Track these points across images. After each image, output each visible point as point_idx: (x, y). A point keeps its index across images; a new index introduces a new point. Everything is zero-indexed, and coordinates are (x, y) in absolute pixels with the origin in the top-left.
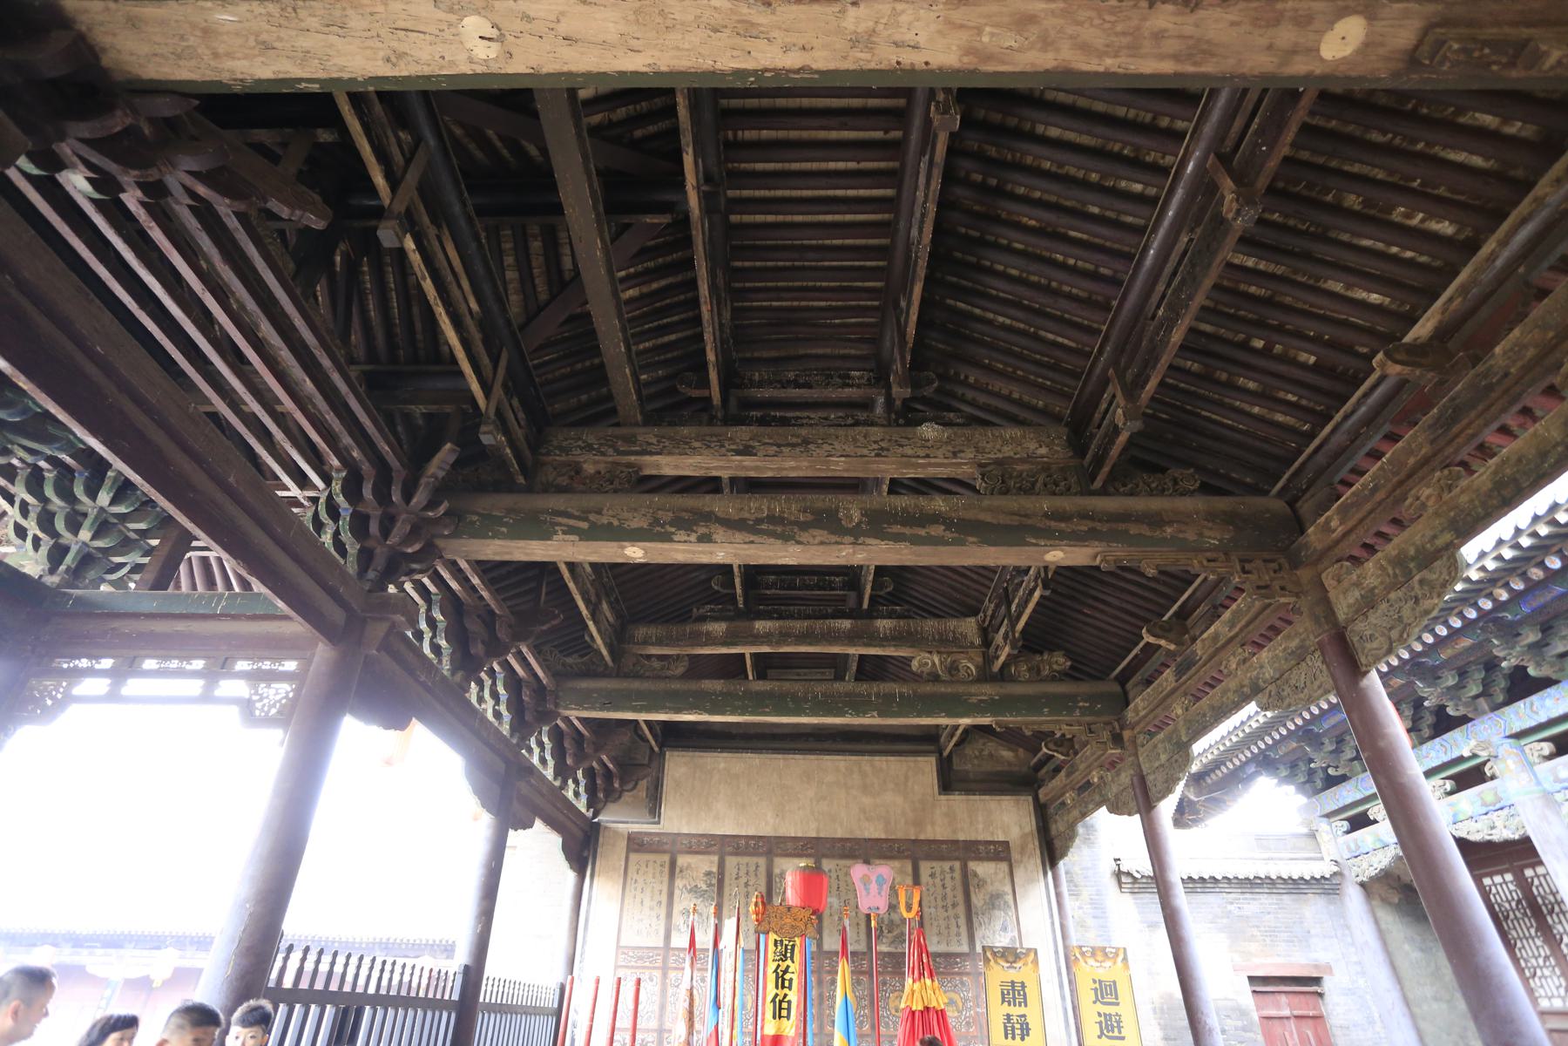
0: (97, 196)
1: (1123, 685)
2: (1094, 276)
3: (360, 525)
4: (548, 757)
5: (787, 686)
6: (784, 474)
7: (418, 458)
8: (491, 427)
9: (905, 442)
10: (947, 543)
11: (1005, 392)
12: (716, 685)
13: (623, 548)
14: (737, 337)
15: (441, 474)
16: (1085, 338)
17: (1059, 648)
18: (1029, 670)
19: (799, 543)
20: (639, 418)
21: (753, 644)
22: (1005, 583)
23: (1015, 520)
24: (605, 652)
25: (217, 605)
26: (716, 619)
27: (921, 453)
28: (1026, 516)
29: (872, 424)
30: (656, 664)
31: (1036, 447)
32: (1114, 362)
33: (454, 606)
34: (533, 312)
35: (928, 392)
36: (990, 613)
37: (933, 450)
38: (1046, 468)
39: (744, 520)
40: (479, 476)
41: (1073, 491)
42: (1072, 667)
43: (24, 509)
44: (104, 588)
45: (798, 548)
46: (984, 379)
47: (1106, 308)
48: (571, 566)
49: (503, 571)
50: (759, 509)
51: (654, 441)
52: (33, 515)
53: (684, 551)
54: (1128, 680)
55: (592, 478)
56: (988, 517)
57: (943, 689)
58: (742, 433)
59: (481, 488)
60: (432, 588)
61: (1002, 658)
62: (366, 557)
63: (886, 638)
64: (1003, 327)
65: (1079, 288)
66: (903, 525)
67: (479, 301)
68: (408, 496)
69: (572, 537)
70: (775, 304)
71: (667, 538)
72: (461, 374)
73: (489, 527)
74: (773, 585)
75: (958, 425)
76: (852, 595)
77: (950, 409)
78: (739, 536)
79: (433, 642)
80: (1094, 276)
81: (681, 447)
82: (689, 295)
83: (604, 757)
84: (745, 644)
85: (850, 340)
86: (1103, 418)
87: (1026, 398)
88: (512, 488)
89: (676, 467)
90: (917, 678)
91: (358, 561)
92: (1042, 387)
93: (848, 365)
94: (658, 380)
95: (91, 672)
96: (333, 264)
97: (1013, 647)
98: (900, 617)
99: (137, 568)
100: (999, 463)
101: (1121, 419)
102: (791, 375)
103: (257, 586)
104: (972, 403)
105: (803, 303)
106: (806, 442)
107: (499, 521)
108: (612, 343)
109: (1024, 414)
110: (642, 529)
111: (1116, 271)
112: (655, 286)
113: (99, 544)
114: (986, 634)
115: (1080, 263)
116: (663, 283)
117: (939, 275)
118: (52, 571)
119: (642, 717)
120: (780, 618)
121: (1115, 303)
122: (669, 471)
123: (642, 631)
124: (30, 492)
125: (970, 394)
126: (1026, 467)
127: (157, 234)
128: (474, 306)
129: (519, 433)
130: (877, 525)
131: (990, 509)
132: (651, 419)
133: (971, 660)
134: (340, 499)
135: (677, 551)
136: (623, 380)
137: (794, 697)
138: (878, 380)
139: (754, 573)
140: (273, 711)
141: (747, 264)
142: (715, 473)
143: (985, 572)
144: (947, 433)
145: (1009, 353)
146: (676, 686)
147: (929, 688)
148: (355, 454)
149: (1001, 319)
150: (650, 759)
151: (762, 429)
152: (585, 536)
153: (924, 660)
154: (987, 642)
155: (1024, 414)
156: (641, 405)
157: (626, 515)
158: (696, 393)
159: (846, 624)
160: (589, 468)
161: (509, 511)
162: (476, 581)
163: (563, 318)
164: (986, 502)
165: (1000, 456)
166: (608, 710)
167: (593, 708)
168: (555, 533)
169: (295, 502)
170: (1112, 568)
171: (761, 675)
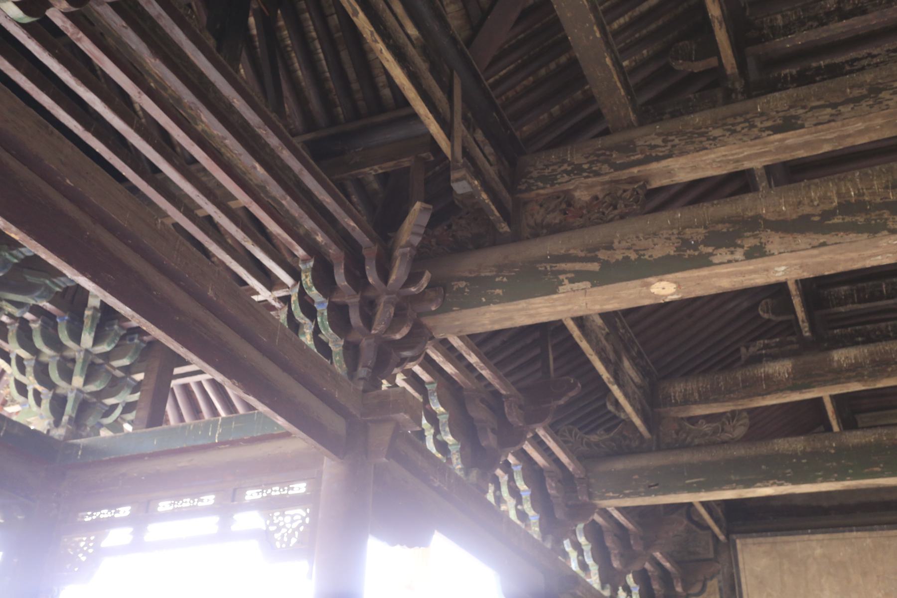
0: (27, 20)
3: (339, 317)
4: (589, 561)
6: (848, 142)
7: (386, 223)
13: (649, 285)
15: (416, 240)
20: (633, 117)
21: (835, 381)
24: (637, 421)
25: (214, 433)
26: (774, 357)
30: (706, 427)
33: (451, 391)
39: (806, 218)
40: (458, 233)
43: (22, 369)
44: (105, 433)
48: (580, 321)
49: (497, 342)
51: (659, 141)
52: (29, 370)
53: (729, 275)
59: (460, 248)
60: (425, 377)
62: (352, 352)
67: (418, 25)
68: (384, 274)
69: (581, 285)
71: (704, 262)
72: (415, 116)
73: (480, 292)
78: (802, 240)
79: (438, 437)
81: (698, 140)
83: (658, 555)
84: (824, 383)
88: (496, 240)
89: (695, 168)
91: (346, 362)
95: (111, 523)
96: (247, 28)
99: (129, 407)
103: (261, 408)
106: (875, 91)
110: (668, 257)
113: (92, 388)
118: (57, 423)
119: (696, 498)
122: (684, 177)
123: (678, 389)
124: (23, 346)
127: (87, 45)
128: (412, 31)
129: (491, 171)
132: (648, 114)
134: (314, 293)
135: (718, 276)
136: (605, 75)
139: (816, 289)
140: (294, 541)
142: (747, 165)
146: (739, 452)
148: (319, 238)
150: (716, 551)
151: (803, 91)
152: (599, 279)
157: (644, 243)
158: (699, 66)
160: (582, 195)
161: (500, 268)
162: (473, 359)
166: (656, 493)
167: (637, 494)
168: (561, 283)
169: (266, 304)
171: (848, 424)
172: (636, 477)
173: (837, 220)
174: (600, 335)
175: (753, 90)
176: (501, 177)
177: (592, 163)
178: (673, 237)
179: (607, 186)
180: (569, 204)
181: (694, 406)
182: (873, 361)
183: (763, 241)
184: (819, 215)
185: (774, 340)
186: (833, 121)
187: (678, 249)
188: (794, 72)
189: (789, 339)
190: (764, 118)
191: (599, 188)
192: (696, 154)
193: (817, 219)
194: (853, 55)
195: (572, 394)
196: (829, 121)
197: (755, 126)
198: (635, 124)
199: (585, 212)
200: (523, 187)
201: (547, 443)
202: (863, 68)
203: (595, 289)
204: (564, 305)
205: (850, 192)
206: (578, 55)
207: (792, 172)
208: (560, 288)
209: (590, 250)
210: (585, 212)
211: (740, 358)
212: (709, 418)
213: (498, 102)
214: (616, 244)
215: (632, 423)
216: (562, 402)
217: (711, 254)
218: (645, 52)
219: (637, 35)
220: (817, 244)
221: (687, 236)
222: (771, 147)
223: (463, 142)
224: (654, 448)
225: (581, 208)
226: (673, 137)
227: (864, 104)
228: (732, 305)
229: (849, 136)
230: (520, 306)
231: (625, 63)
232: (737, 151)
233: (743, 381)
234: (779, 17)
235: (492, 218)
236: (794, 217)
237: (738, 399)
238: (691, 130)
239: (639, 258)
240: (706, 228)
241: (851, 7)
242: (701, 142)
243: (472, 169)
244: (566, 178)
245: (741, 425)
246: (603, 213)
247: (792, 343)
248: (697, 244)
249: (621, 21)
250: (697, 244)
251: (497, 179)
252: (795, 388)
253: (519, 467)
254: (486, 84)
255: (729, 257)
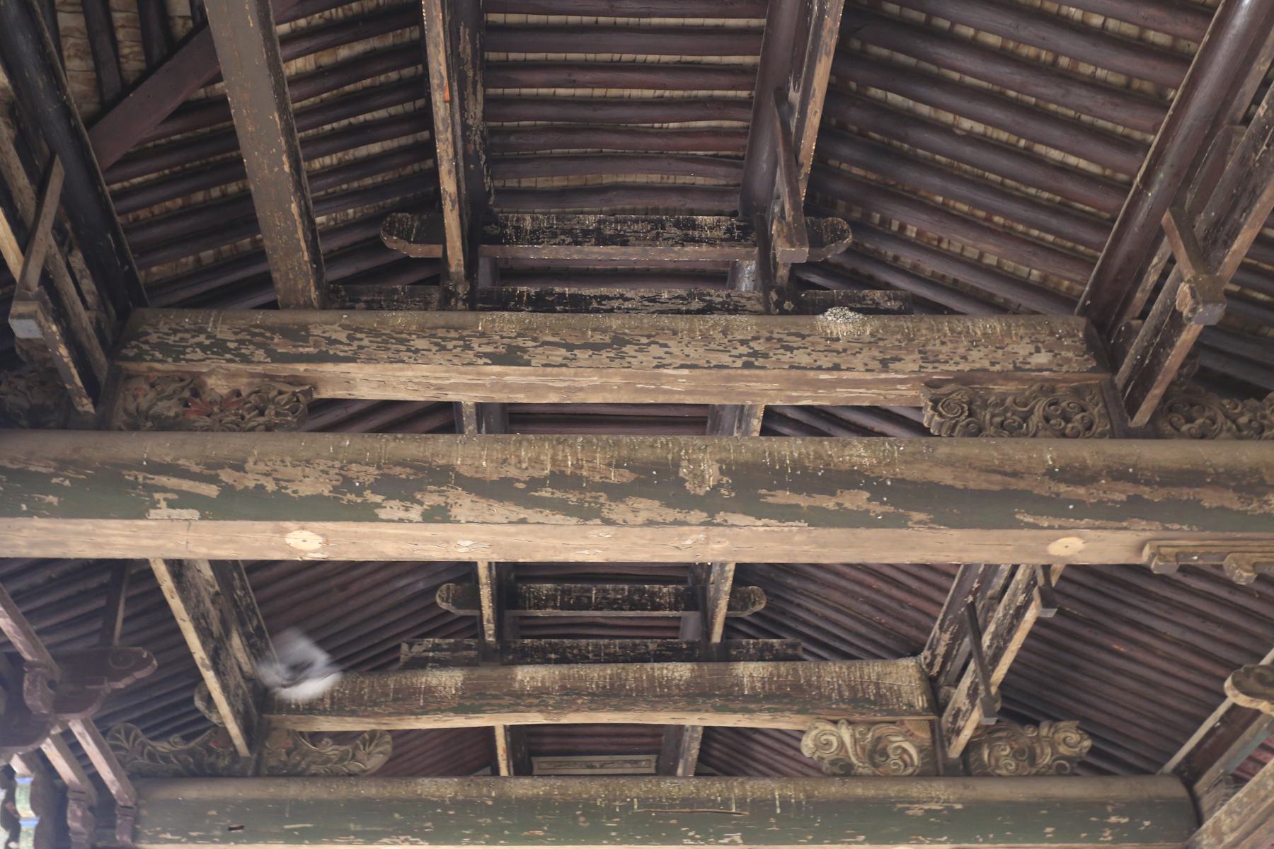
1: (1189, 784)
2: (1138, 46)
5: (575, 787)
6: (578, 398)
8: (32, 307)
9: (796, 342)
10: (871, 523)
11: (972, 253)
12: (444, 788)
13: (284, 532)
14: (493, 150)
16: (1119, 158)
17: (1070, 715)
18: (1016, 754)
19: (608, 522)
20: (314, 294)
21: (513, 708)
22: (971, 596)
23: (995, 483)
24: (234, 729)
26: (443, 664)
27: (825, 362)
28: (1014, 474)
29: (737, 310)
30: (331, 750)
31: (1036, 352)
32: (1174, 202)
34: (113, 94)
35: (834, 252)
36: (941, 650)
37: (843, 359)
38: (1048, 389)
39: (507, 482)
41: (1098, 428)
42: (1093, 751)
45: (606, 532)
46: (933, 232)
47: (1158, 102)
48: (177, 567)
49: (39, 578)
50: (536, 461)
51: (342, 336)
53: (397, 538)
54: (1197, 775)
55: (224, 403)
56: (946, 477)
57: (859, 790)
58: (505, 324)
61: (967, 734)
63: (754, 698)
64: (971, 139)
65: (1108, 67)
66: (796, 490)
69: (186, 513)
70: (561, 91)
71: (366, 514)
74: (549, 601)
75: (887, 312)
76: (691, 619)
77: (873, 283)
78: (500, 511)
80: (1138, 46)
81: (394, 347)
82: (408, 72)
85: (696, 160)
86: (1151, 301)
87: (1009, 265)
88: (68, 421)
89: (383, 384)
90: (812, 769)
92: (1038, 245)
93: (690, 204)
94: (348, 226)
97: (987, 713)
98: (778, 657)
100: (963, 379)
101: (1188, 300)
102: (590, 221)
104: (913, 274)
105: (614, 92)
106: (619, 341)
107: (41, 483)
108: (267, 157)
109: (1002, 292)
110: (320, 497)
111: (1176, 37)
112: (344, 53)
114: (936, 687)
115: (1112, 24)
116: (359, 48)
117: (856, 44)
120: (563, 660)
121: (1174, 95)
125: (908, 258)
126: (1011, 387)
130: (748, 489)
131: (949, 463)
132: (337, 296)
133: (909, 735)
135: (381, 537)
136: (284, 223)
137: (590, 809)
138: (745, 231)
139: (515, 579)
141: (513, 18)
142: (452, 397)
143: (933, 577)
144: (871, 326)
145: (980, 184)
146: (369, 790)
147: (834, 789)
149: (967, 124)
151: (539, 317)
152: (213, 510)
153: (823, 737)
154: (937, 705)
155: (1002, 292)
156: (318, 273)
157: (290, 471)
158: (418, 251)
159: (681, 671)
160: (218, 385)
161: (63, 465)
163: (171, 106)
164: (943, 450)
165: (965, 367)
168: (154, 505)
170: (1171, 569)
171: (522, 768)
172: (214, 813)
173: (545, 493)
174: (204, 594)
175: (479, 301)
176: (99, 330)
177: (241, 342)
178: (332, 472)
179: (257, 380)
180: (196, 393)
181: (321, 718)
182: (563, 687)
183: (449, 501)
184: (524, 482)
185: (447, 641)
186: (566, 366)
187: (335, 489)
188: (533, 291)
189: (466, 641)
190: (485, 340)
191: (245, 380)
192: (388, 366)
193: (521, 486)
194: (603, 290)
195: (139, 675)
196: (561, 365)
197: (471, 348)
198: (315, 304)
199: (216, 409)
200: (132, 353)
201: (84, 745)
202: (611, 311)
203: (204, 523)
204: (152, 538)
205: (566, 461)
206: (252, 187)
207: (514, 419)
208: (152, 511)
209: (209, 466)
210: (216, 409)
211: (398, 659)
212: (339, 737)
213: (119, 220)
214: (250, 465)
215: (225, 730)
216: (121, 685)
217: (379, 506)
218: (351, 211)
219: (345, 186)
220: (515, 519)
221: (351, 474)
222: (487, 381)
223: (46, 261)
224: (250, 773)
225: (212, 403)
226: (362, 336)
227: (604, 354)
228: (403, 582)
229: (581, 389)
230: (82, 528)
231: (319, 220)
232: (443, 375)
233: (396, 691)
234: (528, 218)
235: (68, 386)
236: (495, 477)
237: (382, 715)
238: (387, 332)
239: (279, 490)
240: (379, 468)
241: (612, 232)
242: (398, 351)
243: (50, 305)
244: (199, 354)
245: (380, 752)
246: (243, 418)
247: (469, 647)
248: (363, 487)
249: (327, 160)
250: (363, 487)
251: (91, 331)
252: (460, 710)
253: (28, 781)
254: (107, 189)
255: (402, 514)
